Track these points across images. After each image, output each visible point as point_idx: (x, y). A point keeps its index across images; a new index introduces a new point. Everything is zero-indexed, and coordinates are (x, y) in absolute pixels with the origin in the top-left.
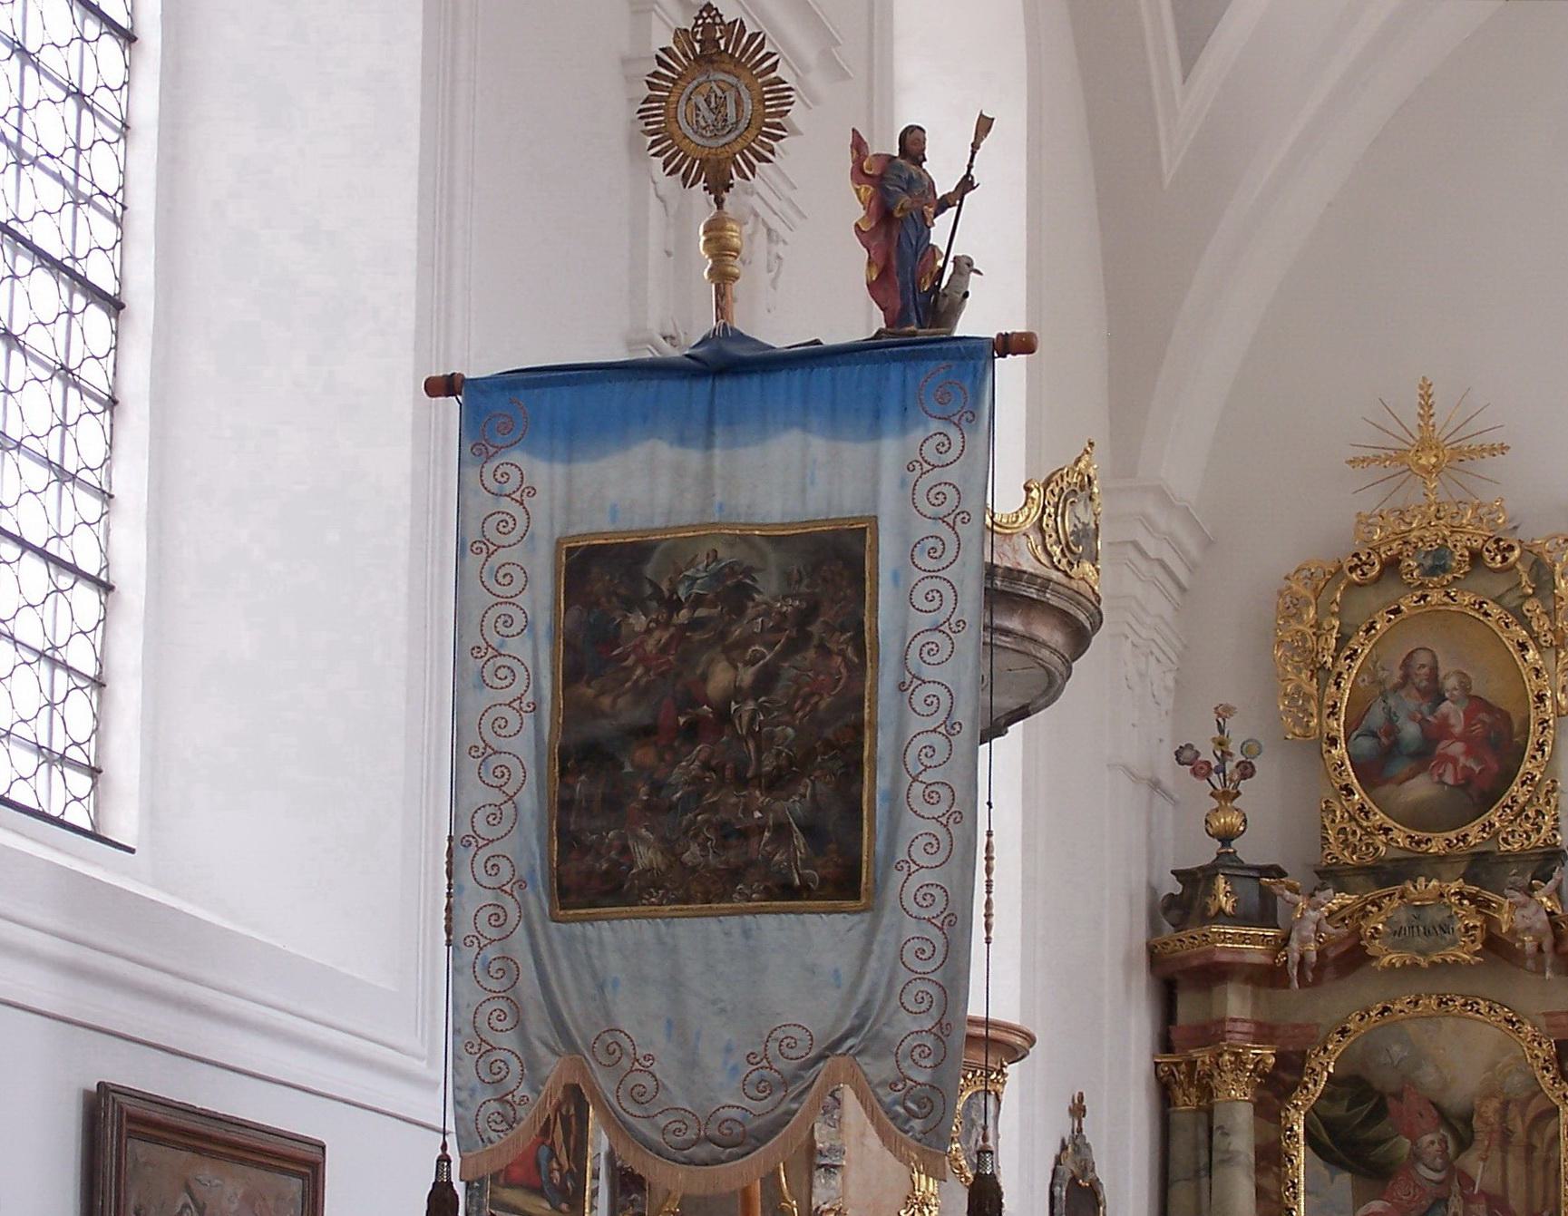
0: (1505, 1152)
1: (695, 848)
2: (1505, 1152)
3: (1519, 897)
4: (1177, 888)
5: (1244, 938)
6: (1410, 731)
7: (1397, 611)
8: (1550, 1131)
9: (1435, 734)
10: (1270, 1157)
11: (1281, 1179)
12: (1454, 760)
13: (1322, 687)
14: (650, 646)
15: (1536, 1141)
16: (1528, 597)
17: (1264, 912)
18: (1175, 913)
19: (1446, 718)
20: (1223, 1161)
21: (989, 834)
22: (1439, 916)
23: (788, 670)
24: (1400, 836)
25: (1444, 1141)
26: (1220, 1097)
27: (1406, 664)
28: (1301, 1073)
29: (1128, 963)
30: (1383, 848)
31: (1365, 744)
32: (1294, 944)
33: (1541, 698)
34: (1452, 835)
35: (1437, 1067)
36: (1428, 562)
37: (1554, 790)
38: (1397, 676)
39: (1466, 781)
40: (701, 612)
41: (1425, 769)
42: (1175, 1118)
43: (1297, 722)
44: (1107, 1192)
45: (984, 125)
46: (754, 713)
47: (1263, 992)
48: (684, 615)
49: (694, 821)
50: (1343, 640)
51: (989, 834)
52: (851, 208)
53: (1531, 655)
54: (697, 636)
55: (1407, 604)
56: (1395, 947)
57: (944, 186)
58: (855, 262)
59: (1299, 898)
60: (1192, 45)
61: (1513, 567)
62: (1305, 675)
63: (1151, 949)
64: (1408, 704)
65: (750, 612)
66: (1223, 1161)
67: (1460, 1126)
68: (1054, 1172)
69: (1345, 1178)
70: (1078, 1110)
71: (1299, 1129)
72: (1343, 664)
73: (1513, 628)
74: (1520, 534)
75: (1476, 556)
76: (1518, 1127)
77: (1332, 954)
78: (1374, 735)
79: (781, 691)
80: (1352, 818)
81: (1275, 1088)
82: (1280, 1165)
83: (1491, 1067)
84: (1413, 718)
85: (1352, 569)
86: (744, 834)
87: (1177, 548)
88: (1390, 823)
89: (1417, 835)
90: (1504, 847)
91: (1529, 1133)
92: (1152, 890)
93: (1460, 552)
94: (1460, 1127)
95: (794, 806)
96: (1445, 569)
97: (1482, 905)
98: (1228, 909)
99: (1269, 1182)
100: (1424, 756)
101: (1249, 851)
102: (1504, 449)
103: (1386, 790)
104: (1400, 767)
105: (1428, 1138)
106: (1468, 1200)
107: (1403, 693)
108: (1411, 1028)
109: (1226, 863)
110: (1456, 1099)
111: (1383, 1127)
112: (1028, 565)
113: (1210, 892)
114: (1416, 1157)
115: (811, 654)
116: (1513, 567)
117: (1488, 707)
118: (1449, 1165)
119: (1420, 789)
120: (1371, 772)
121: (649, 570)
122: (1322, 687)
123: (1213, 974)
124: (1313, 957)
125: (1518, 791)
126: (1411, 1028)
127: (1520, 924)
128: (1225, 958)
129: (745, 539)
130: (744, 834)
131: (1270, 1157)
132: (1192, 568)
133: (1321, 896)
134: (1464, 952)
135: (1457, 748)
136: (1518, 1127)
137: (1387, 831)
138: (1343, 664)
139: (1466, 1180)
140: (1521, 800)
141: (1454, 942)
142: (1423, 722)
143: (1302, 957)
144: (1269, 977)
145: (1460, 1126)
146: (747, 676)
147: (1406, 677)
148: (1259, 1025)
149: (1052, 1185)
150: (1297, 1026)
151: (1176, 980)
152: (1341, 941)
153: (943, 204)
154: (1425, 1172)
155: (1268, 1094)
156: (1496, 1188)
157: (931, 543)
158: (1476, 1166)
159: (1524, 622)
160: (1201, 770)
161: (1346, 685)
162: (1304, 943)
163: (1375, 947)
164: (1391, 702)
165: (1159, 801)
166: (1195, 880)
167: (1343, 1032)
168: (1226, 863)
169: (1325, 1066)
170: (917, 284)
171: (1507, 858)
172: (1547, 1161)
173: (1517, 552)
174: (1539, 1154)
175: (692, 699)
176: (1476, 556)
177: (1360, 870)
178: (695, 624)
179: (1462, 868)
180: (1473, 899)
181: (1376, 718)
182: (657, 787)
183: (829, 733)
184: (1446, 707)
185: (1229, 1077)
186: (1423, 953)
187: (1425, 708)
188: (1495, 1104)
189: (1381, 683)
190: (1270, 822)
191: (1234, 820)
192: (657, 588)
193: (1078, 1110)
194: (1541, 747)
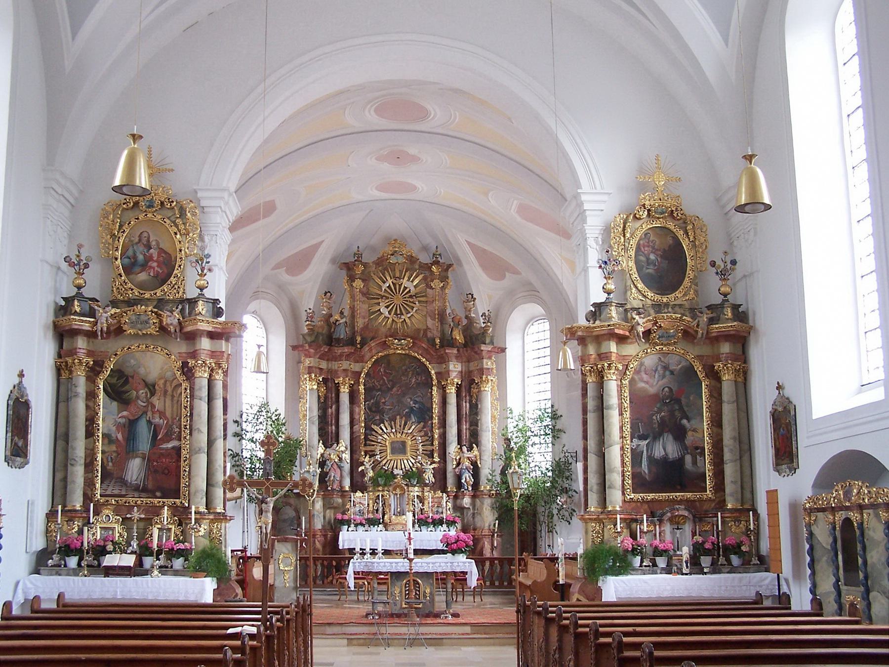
3: (169, 313)
4: (63, 303)
5: (83, 321)
6: (141, 257)
8: (179, 392)
10: (91, 396)
11: (95, 403)
12: (154, 268)
13: (114, 241)
17: (92, 313)
18: (62, 312)
22: (143, 318)
26: (75, 374)
27: (140, 236)
29: (46, 327)
31: (126, 261)
33: (181, 250)
38: (137, 240)
39: (156, 276)
43: (105, 252)
44: (33, 404)
47: (91, 340)
50: (121, 226)
53: (178, 236)
55: (141, 217)
56: (132, 328)
60: (74, 34)
61: (173, 208)
62: (109, 237)
63: (54, 323)
64: (140, 249)
69: (115, 404)
70: (21, 375)
71: (101, 387)
72: (120, 235)
74: (176, 198)
75: (162, 203)
76: (170, 389)
77: (112, 328)
81: (94, 372)
82: (95, 398)
83: (162, 369)
87: (71, 194)
89: (142, 292)
92: (56, 304)
93: (157, 202)
94: (151, 388)
96: (153, 207)
97: (159, 316)
98: (78, 311)
99: (91, 404)
100: (144, 266)
101: (87, 292)
102: (172, 170)
103: (131, 277)
104: (137, 269)
106: (153, 413)
108: (137, 355)
109: (79, 296)
111: (127, 388)
113: (73, 305)
114: (138, 397)
116: (173, 208)
117: (166, 253)
118: (148, 401)
119: (142, 276)
120: (128, 270)
122: (114, 241)
123: (75, 333)
124: (105, 329)
126: (137, 355)
127: (169, 322)
128: (76, 327)
131: (91, 396)
132: (76, 199)
133: (107, 309)
134: (152, 330)
135: (155, 264)
136: (170, 389)
138: (120, 235)
139: (153, 406)
144: (91, 335)
147: (140, 240)
148: (89, 351)
151: (62, 334)
152: (115, 324)
154: (140, 402)
155: (91, 374)
156: (162, 409)
158: (155, 400)
159: (176, 226)
160: (72, 265)
161: (121, 241)
162: (103, 324)
163: (125, 327)
165: (60, 273)
166: (69, 300)
167: (116, 355)
168: (79, 296)
171: (168, 301)
174: (175, 399)
176: (162, 203)
177: (123, 301)
179: (155, 303)
180: (156, 313)
181: (130, 253)
184: (152, 251)
185: (77, 367)
188: (162, 381)
190: (94, 283)
191: (81, 281)
193: (21, 375)
194: (180, 266)
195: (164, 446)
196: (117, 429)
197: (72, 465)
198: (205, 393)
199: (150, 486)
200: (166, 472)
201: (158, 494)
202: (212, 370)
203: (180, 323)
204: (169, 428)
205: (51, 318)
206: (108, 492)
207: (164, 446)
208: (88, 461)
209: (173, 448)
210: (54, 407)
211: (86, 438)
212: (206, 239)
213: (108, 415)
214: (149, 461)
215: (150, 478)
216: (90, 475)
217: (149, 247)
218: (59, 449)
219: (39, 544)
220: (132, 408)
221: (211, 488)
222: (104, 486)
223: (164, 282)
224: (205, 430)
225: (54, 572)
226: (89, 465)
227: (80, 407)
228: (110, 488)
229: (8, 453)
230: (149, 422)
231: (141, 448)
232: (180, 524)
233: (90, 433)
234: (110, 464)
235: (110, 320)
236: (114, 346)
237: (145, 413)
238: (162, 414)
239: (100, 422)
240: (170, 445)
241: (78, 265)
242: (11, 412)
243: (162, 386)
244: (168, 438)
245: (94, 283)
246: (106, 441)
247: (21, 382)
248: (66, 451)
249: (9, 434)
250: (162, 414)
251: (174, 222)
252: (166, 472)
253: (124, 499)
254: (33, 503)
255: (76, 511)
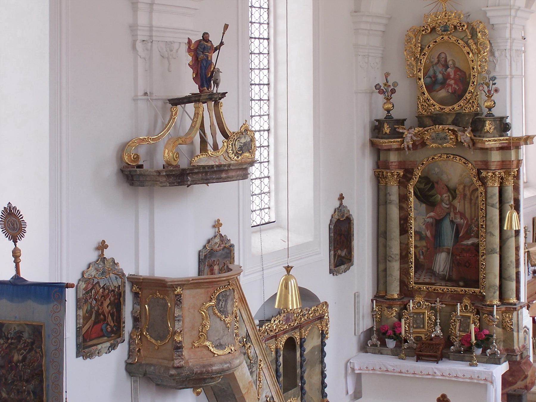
0: (464, 200)
1: (13, 394)
2: (464, 200)
6: (440, 76)
7: (436, 42)
8: (476, 195)
9: (446, 77)
10: (403, 198)
11: (408, 205)
12: (451, 86)
13: (417, 63)
14: (4, 347)
15: (473, 198)
16: (470, 39)
19: (449, 74)
20: (389, 203)
21: (66, 399)
22: (443, 135)
23: (29, 357)
24: (437, 106)
25: (449, 196)
27: (438, 57)
28: (412, 175)
30: (433, 110)
31: (428, 80)
32: (405, 143)
33: (473, 68)
34: (450, 107)
35: (447, 176)
36: (443, 29)
37: (477, 95)
39: (454, 92)
40: (13, 341)
41: (443, 88)
42: (381, 187)
45: (226, 27)
46: (22, 366)
48: (10, 341)
49: (12, 388)
50: (422, 49)
51: (66, 399)
52: (189, 59)
53: (471, 55)
54: (12, 346)
56: (434, 143)
57: (216, 44)
58: (189, 73)
59: (405, 131)
64: (440, 68)
65: (22, 342)
66: (389, 203)
67: (453, 192)
68: (331, 220)
69: (424, 205)
73: (466, 48)
76: (468, 193)
78: (430, 77)
79: (27, 360)
80: (425, 101)
81: (403, 182)
83: (461, 175)
84: (440, 73)
85: (423, 31)
86: (22, 392)
88: (435, 103)
89: (442, 107)
90: (464, 111)
91: (471, 196)
94: (453, 192)
95: (31, 387)
96: (447, 31)
100: (444, 84)
101: (396, 114)
103: (434, 93)
104: (437, 87)
105: (445, 195)
106: (455, 214)
107: (438, 65)
109: (389, 118)
110: (452, 184)
111: (433, 192)
112: (224, 163)
114: (442, 200)
115: (33, 352)
118: (450, 204)
119: (442, 93)
120: (430, 88)
121: (4, 329)
123: (463, 38)
125: (468, 96)
129: (20, 325)
130: (22, 392)
135: (452, 82)
136: (468, 193)
137: (434, 105)
138: (422, 57)
139: (455, 208)
140: (468, 98)
141: (448, 142)
142: (443, 74)
143: (408, 146)
145: (453, 192)
146: (21, 357)
147: (439, 61)
149: (330, 225)
150: (411, 161)
153: (216, 49)
156: (462, 211)
157: (55, 330)
158: (456, 203)
159: (469, 46)
160: (381, 92)
163: (428, 142)
164: (435, 68)
167: (423, 164)
168: (389, 118)
169: (418, 173)
170: (206, 75)
172: (475, 204)
173: (466, 27)
175: (11, 362)
176: (455, 27)
178: (12, 343)
181: (431, 73)
182: (6, 379)
183: (36, 372)
184: (449, 70)
186: (440, 144)
187: (444, 70)
188: (462, 186)
189: (432, 62)
191: (390, 106)
192: (5, 334)
193: (341, 198)
194: (473, 83)
195: (465, 243)
196: (427, 227)
197: (389, 261)
198: (496, 200)
199: (454, 277)
200: (467, 265)
201: (461, 283)
202: (502, 178)
203: (472, 140)
204: (469, 226)
205: (368, 137)
206: (420, 281)
207: (465, 243)
208: (404, 254)
209: (473, 244)
210: (376, 211)
211: (400, 235)
212: (497, 54)
213: (419, 217)
214: (453, 254)
215: (454, 269)
216: (406, 266)
217: (446, 66)
218: (381, 245)
219: (366, 323)
220: (438, 209)
221: (503, 281)
222: (417, 275)
223: (460, 96)
224: (497, 233)
225: (377, 351)
226: (404, 257)
227: (394, 213)
228: (422, 277)
229: (332, 267)
230: (452, 222)
231: (446, 244)
232: (478, 313)
233: (404, 230)
234: (422, 257)
235: (415, 138)
236: (420, 156)
237: (448, 214)
238: (462, 215)
239: (412, 221)
240: (470, 242)
241: (386, 91)
242: (332, 235)
243: (461, 191)
244: (468, 236)
245: (404, 105)
246: (418, 238)
247: (341, 204)
248: (385, 246)
249: (332, 252)
250: (462, 215)
251: (467, 43)
252: (467, 265)
253: (434, 287)
254: (358, 296)
255: (395, 299)
